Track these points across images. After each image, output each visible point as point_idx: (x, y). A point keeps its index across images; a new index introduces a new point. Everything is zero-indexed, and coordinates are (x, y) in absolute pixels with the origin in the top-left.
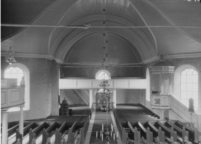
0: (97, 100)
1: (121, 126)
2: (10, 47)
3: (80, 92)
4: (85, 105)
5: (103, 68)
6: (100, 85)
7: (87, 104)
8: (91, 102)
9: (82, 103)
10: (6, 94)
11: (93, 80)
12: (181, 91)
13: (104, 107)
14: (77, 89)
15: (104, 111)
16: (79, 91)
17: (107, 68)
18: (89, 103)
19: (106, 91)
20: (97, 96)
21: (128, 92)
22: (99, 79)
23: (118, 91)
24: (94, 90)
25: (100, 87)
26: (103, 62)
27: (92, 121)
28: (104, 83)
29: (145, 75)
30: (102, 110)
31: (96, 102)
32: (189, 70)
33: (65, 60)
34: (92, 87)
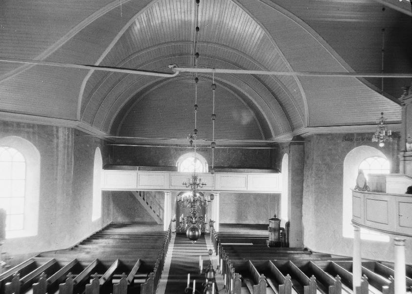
0: (178, 216)
1: (232, 271)
2: (381, 112)
3: (144, 195)
4: (154, 224)
5: (192, 150)
6: (186, 184)
7: (157, 220)
8: (168, 220)
9: (148, 220)
10: (399, 223)
11: (173, 173)
12: (25, 180)
13: (194, 229)
14: (137, 192)
15: (194, 238)
16: (142, 195)
17: (203, 150)
18: (162, 220)
19: (198, 195)
20: (179, 208)
21: (243, 200)
22: (184, 171)
23: (224, 194)
24: (173, 191)
25: (185, 188)
26: (191, 137)
27: (168, 261)
28: (195, 182)
29: (280, 166)
30: (189, 235)
31: (177, 220)
32: (376, 159)
33: (113, 131)
34: (170, 187)
